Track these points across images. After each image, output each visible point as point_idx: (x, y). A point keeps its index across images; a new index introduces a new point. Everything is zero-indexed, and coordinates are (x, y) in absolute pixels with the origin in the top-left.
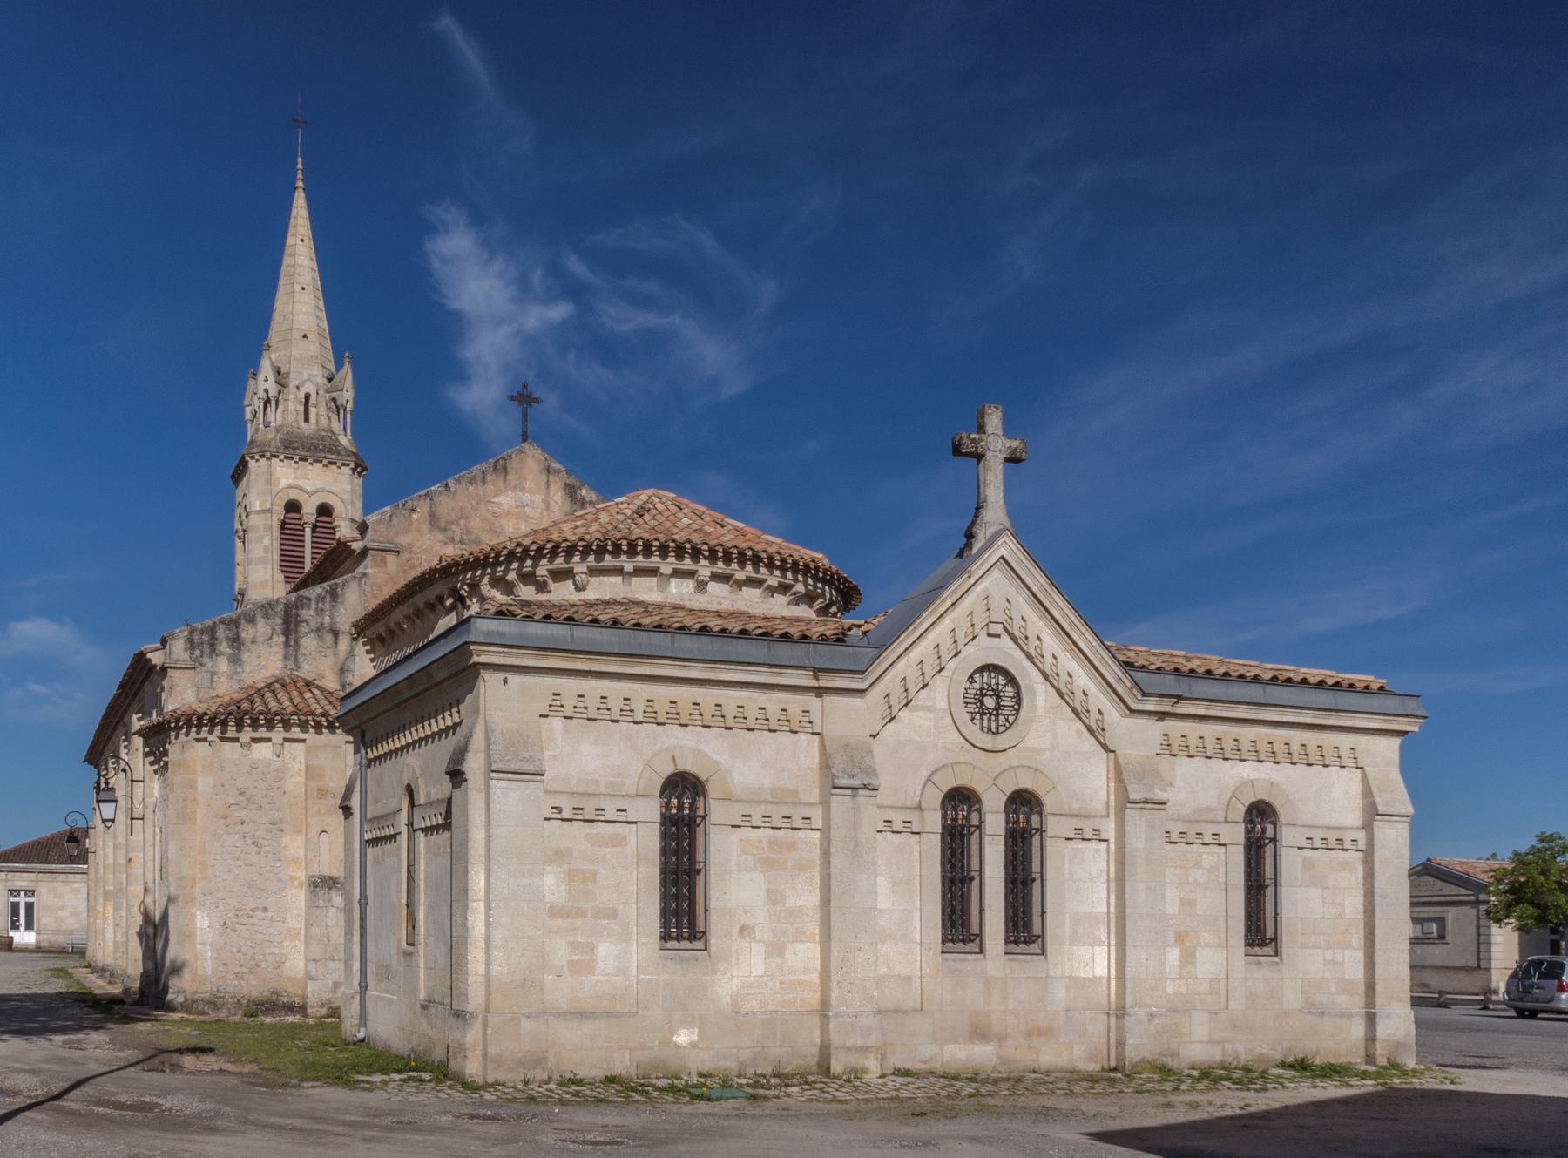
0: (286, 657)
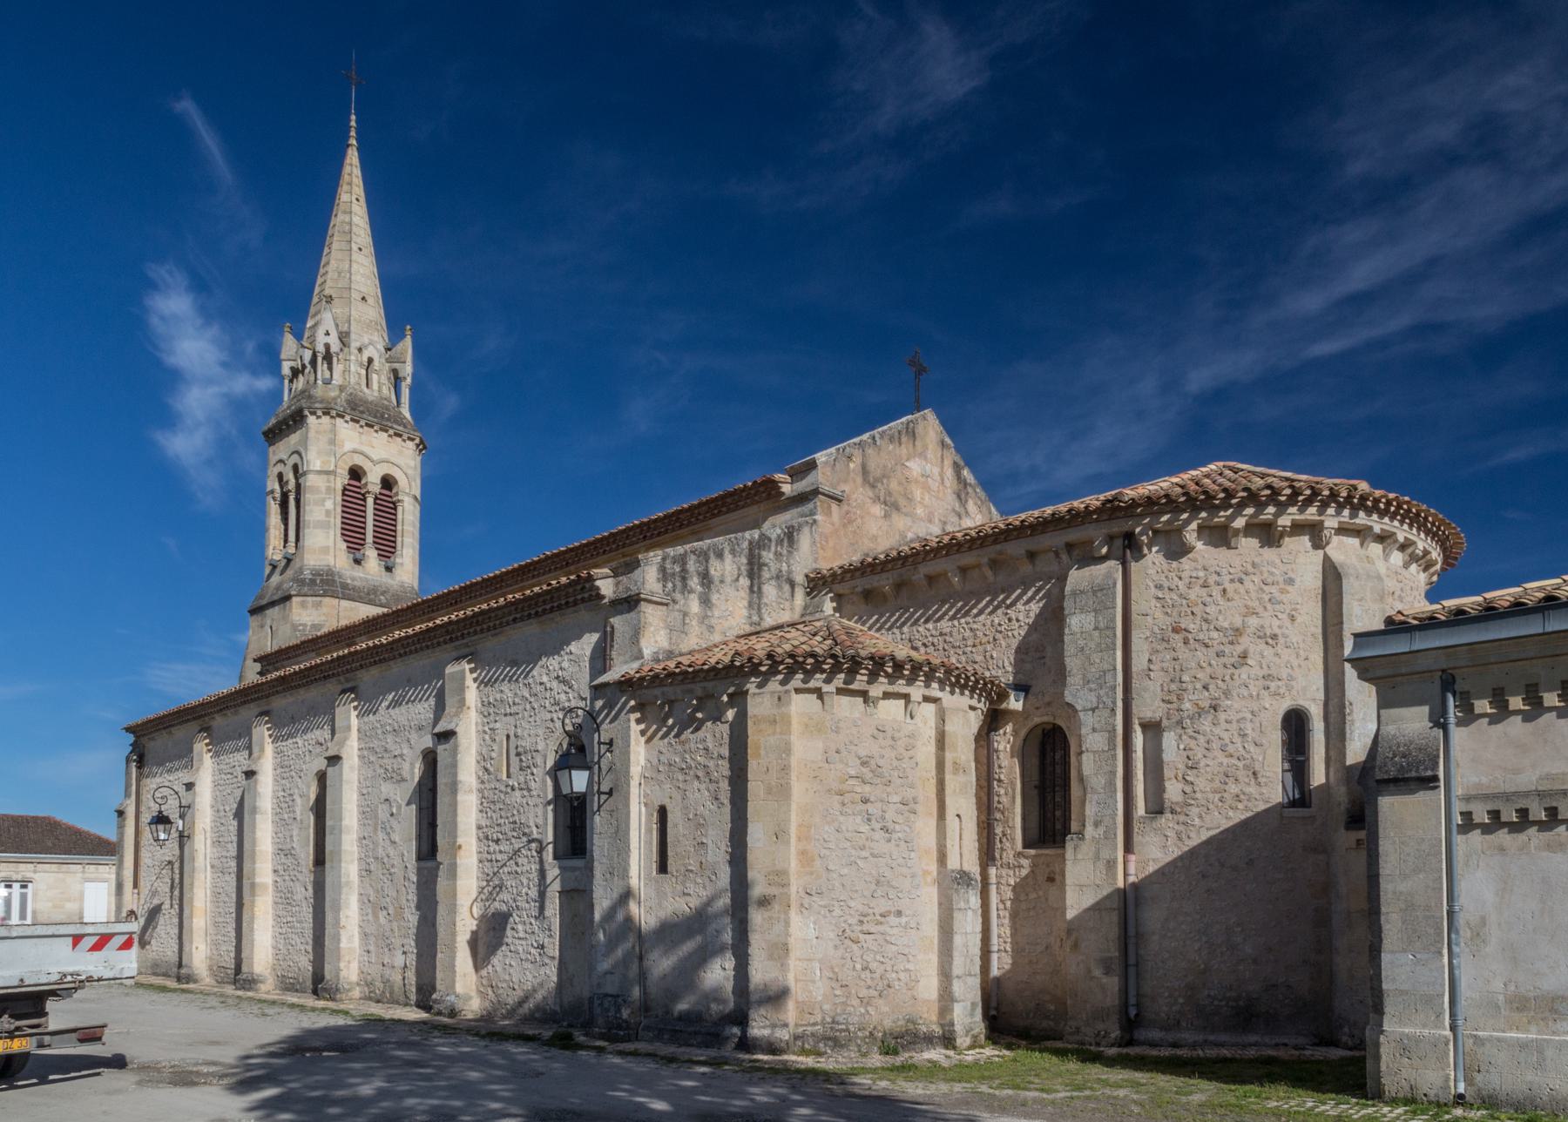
0: (750, 605)
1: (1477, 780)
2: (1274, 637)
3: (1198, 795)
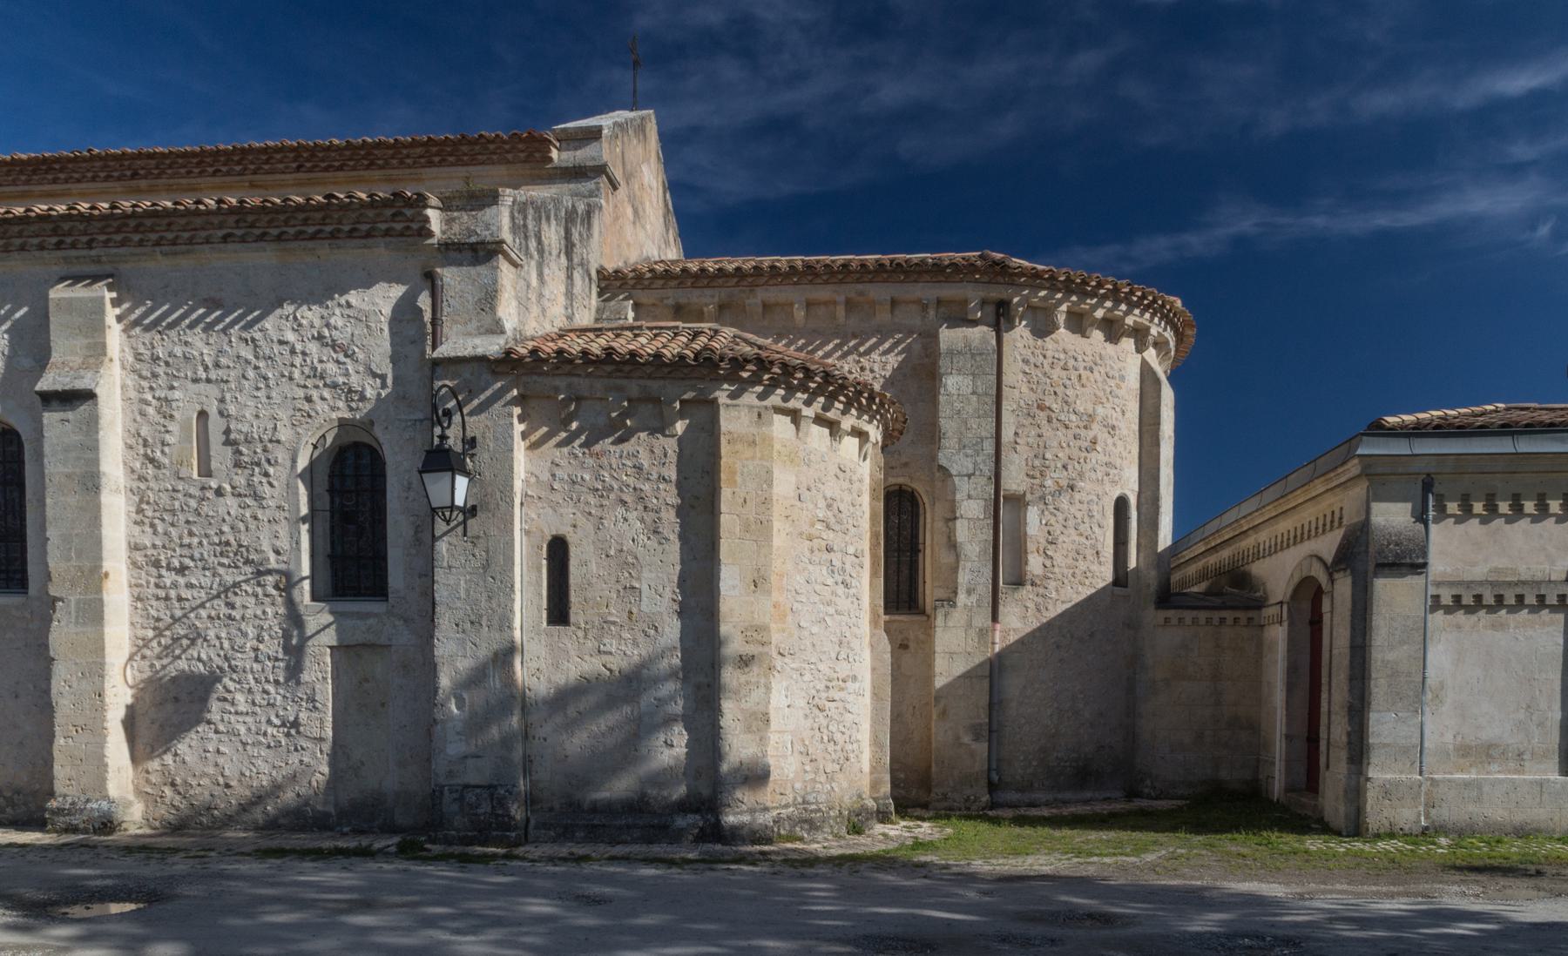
1: (1443, 569)
2: (1113, 427)
3: (1056, 570)
